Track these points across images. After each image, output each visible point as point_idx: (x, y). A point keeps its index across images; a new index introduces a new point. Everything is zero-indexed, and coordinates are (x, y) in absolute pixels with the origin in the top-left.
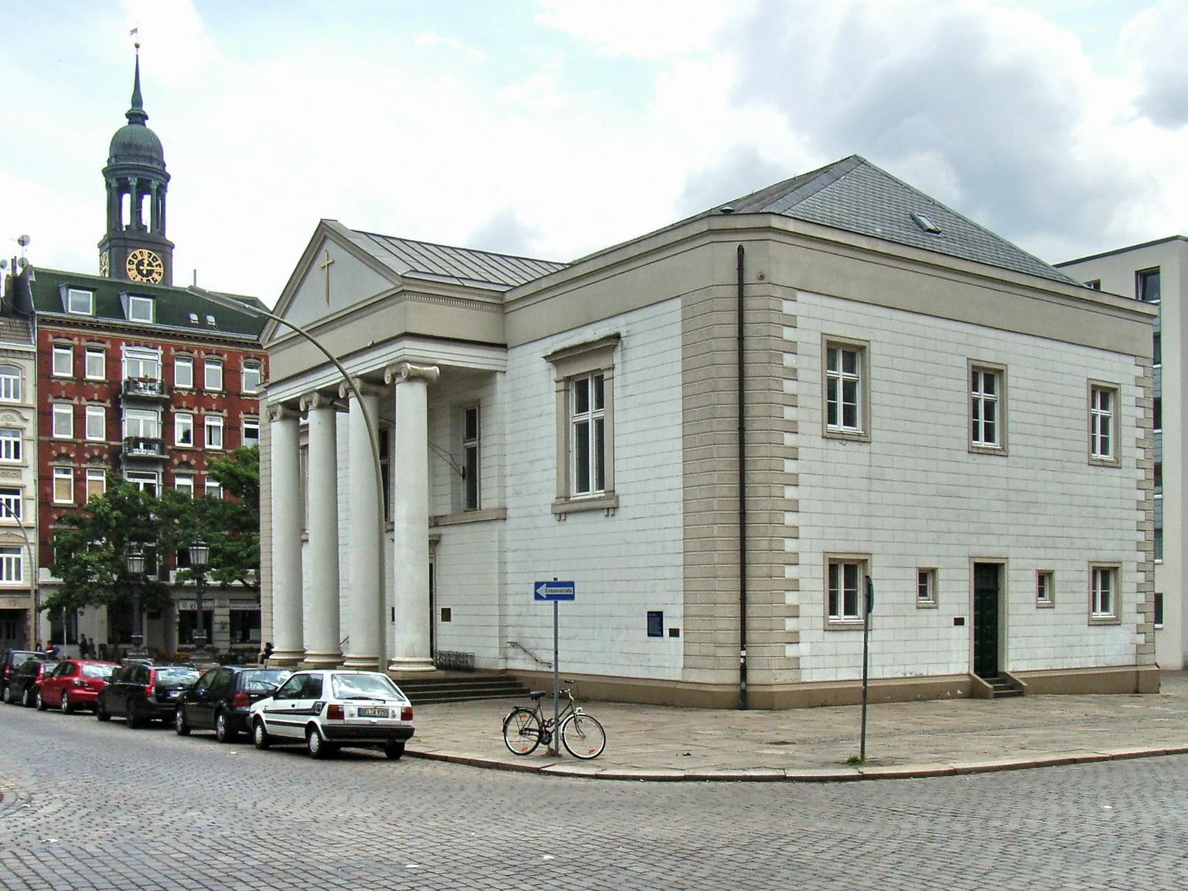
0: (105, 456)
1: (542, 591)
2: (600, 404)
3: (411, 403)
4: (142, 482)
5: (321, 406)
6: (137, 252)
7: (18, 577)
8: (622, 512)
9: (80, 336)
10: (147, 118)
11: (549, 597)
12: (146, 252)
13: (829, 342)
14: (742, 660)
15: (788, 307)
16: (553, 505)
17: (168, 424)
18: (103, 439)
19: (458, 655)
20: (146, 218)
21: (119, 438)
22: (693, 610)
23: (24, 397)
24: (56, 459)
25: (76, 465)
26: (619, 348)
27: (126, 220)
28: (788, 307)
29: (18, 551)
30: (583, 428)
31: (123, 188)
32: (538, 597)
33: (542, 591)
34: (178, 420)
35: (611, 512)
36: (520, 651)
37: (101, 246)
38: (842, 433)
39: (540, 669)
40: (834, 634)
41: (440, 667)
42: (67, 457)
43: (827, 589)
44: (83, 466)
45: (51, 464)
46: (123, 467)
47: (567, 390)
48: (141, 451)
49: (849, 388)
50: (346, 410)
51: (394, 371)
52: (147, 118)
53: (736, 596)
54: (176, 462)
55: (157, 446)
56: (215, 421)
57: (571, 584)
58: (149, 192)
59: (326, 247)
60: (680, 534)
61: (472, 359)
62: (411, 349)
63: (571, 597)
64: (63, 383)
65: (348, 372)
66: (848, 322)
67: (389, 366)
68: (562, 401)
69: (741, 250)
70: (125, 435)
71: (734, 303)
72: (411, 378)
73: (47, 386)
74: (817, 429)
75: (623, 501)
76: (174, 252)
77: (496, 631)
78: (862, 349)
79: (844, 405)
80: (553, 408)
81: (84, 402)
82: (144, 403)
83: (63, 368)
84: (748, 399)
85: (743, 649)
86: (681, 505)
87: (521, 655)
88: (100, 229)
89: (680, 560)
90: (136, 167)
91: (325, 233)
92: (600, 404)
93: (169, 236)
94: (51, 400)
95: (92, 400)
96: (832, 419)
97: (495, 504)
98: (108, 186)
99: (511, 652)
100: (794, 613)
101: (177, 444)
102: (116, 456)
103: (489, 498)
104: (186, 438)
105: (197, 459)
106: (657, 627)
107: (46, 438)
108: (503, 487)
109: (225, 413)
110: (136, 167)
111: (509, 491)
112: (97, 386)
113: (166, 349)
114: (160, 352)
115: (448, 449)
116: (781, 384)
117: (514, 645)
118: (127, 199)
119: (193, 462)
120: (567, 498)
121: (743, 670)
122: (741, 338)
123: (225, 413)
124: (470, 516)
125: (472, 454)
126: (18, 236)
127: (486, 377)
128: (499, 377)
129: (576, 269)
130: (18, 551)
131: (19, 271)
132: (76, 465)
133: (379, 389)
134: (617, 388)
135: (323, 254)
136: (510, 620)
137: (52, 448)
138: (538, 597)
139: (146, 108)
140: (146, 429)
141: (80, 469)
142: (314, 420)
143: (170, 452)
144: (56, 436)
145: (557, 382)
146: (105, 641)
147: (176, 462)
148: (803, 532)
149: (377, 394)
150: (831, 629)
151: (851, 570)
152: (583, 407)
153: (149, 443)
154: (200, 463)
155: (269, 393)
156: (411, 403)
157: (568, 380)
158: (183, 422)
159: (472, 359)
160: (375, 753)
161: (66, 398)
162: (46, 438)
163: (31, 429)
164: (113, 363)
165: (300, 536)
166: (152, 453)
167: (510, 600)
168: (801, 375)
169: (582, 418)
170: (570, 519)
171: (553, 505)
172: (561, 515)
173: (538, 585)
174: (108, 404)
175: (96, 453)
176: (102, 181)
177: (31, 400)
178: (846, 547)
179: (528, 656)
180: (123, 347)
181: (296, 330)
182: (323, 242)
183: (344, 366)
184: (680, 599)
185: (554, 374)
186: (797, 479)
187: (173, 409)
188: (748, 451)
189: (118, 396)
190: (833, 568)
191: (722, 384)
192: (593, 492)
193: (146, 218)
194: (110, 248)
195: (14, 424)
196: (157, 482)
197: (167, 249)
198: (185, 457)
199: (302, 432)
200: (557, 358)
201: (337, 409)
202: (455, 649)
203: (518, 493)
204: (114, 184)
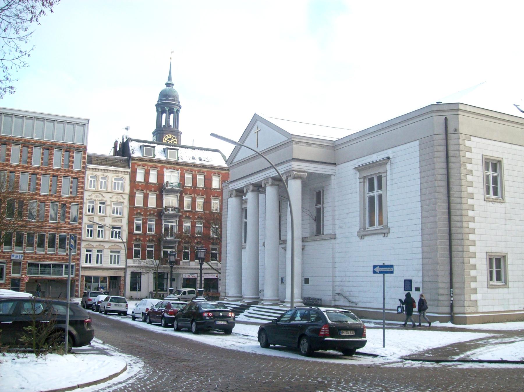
0: (156, 214)
1: (377, 269)
2: (380, 187)
3: (295, 188)
4: (170, 224)
5: (253, 191)
6: (167, 136)
7: (118, 263)
8: (390, 235)
9: (148, 165)
10: (173, 85)
11: (380, 273)
12: (171, 135)
13: (485, 159)
14: (451, 302)
15: (467, 143)
16: (358, 232)
17: (181, 201)
18: (155, 207)
19: (316, 299)
20: (171, 123)
21: (162, 206)
22: (427, 279)
23: (124, 190)
24: (135, 215)
25: (144, 217)
26: (389, 163)
27: (164, 123)
28: (467, 143)
29: (119, 252)
30: (372, 199)
31: (163, 111)
32: (375, 272)
33: (377, 269)
34: (185, 199)
35: (386, 235)
36: (341, 297)
37: (153, 133)
38: (493, 199)
39: (351, 305)
40: (492, 290)
41: (306, 304)
42: (140, 214)
43: (489, 270)
44: (147, 217)
45: (134, 217)
46: (163, 218)
47: (364, 182)
48: (171, 212)
49: (495, 179)
50: (264, 192)
51: (287, 175)
52: (173, 85)
53: (448, 273)
54: (184, 216)
55: (176, 210)
56: (200, 201)
57: (392, 266)
58: (173, 113)
59: (257, 124)
60: (420, 244)
61: (322, 170)
62: (296, 165)
63: (392, 272)
64: (140, 184)
65: (279, 171)
66: (495, 150)
67: (285, 173)
68: (362, 187)
69: (446, 119)
70: (164, 206)
71: (444, 142)
72: (295, 178)
73: (134, 186)
74: (482, 197)
75: (392, 230)
76: (182, 135)
77: (331, 288)
78: (500, 162)
79: (495, 188)
80: (358, 190)
81: (148, 192)
82: (171, 192)
83: (140, 177)
84: (451, 184)
85: (451, 297)
86: (421, 231)
87: (342, 299)
88: (154, 127)
89: (420, 256)
90: (167, 104)
91: (256, 119)
92: (380, 187)
93: (180, 129)
94: (135, 191)
95: (151, 191)
96: (488, 193)
97: (330, 232)
98: (157, 110)
99: (337, 297)
100: (474, 279)
101: (185, 209)
102: (160, 214)
103: (327, 229)
104: (188, 207)
105: (193, 215)
106: (409, 287)
107: (132, 206)
108: (334, 225)
109: (205, 196)
110: (167, 104)
111: (337, 227)
112: (153, 185)
113: (182, 170)
114: (179, 171)
115: (308, 209)
116: (466, 177)
117: (339, 294)
118: (164, 115)
119: (191, 216)
120: (365, 229)
121: (452, 306)
122: (447, 157)
123: (205, 196)
124: (318, 237)
125: (319, 212)
126: (126, 127)
127: (327, 177)
128: (333, 177)
129: (235, 183)
130: (119, 252)
131: (125, 140)
132: (144, 217)
133: (279, 182)
134: (388, 181)
135: (255, 127)
136: (337, 283)
137: (134, 210)
138: (375, 272)
139: (173, 81)
140: (172, 203)
141: (145, 219)
142: (250, 196)
143: (182, 212)
144: (136, 205)
145: (360, 179)
146: (152, 291)
147: (184, 216)
148: (477, 243)
149: (278, 185)
150: (490, 287)
151: (498, 260)
152: (371, 189)
153: (174, 209)
154: (194, 216)
155: (230, 186)
156: (295, 188)
157: (364, 178)
158: (187, 200)
159: (322, 170)
160: (332, 352)
161: (141, 190)
162: (132, 206)
163: (126, 202)
164: (160, 176)
165: (241, 247)
166: (175, 212)
167: (337, 274)
168: (474, 173)
169: (371, 194)
170: (366, 238)
171: (358, 232)
172: (362, 237)
173: (375, 267)
174: (158, 192)
175: (152, 212)
176: (155, 109)
177: (127, 191)
178: (497, 250)
179: (345, 300)
180: (165, 170)
181: (257, 152)
182: (256, 122)
183: (278, 168)
184: (420, 274)
185: (358, 175)
186: (474, 219)
187: (184, 195)
188: (452, 207)
189: (161, 189)
190: (491, 259)
191: (439, 177)
192: (377, 226)
193: (171, 123)
194: (157, 134)
195: (119, 200)
196: (175, 224)
197: (179, 134)
198: (188, 214)
199: (243, 202)
200: (359, 169)
201: (259, 192)
202: (311, 296)
203: (341, 227)
204: (160, 110)
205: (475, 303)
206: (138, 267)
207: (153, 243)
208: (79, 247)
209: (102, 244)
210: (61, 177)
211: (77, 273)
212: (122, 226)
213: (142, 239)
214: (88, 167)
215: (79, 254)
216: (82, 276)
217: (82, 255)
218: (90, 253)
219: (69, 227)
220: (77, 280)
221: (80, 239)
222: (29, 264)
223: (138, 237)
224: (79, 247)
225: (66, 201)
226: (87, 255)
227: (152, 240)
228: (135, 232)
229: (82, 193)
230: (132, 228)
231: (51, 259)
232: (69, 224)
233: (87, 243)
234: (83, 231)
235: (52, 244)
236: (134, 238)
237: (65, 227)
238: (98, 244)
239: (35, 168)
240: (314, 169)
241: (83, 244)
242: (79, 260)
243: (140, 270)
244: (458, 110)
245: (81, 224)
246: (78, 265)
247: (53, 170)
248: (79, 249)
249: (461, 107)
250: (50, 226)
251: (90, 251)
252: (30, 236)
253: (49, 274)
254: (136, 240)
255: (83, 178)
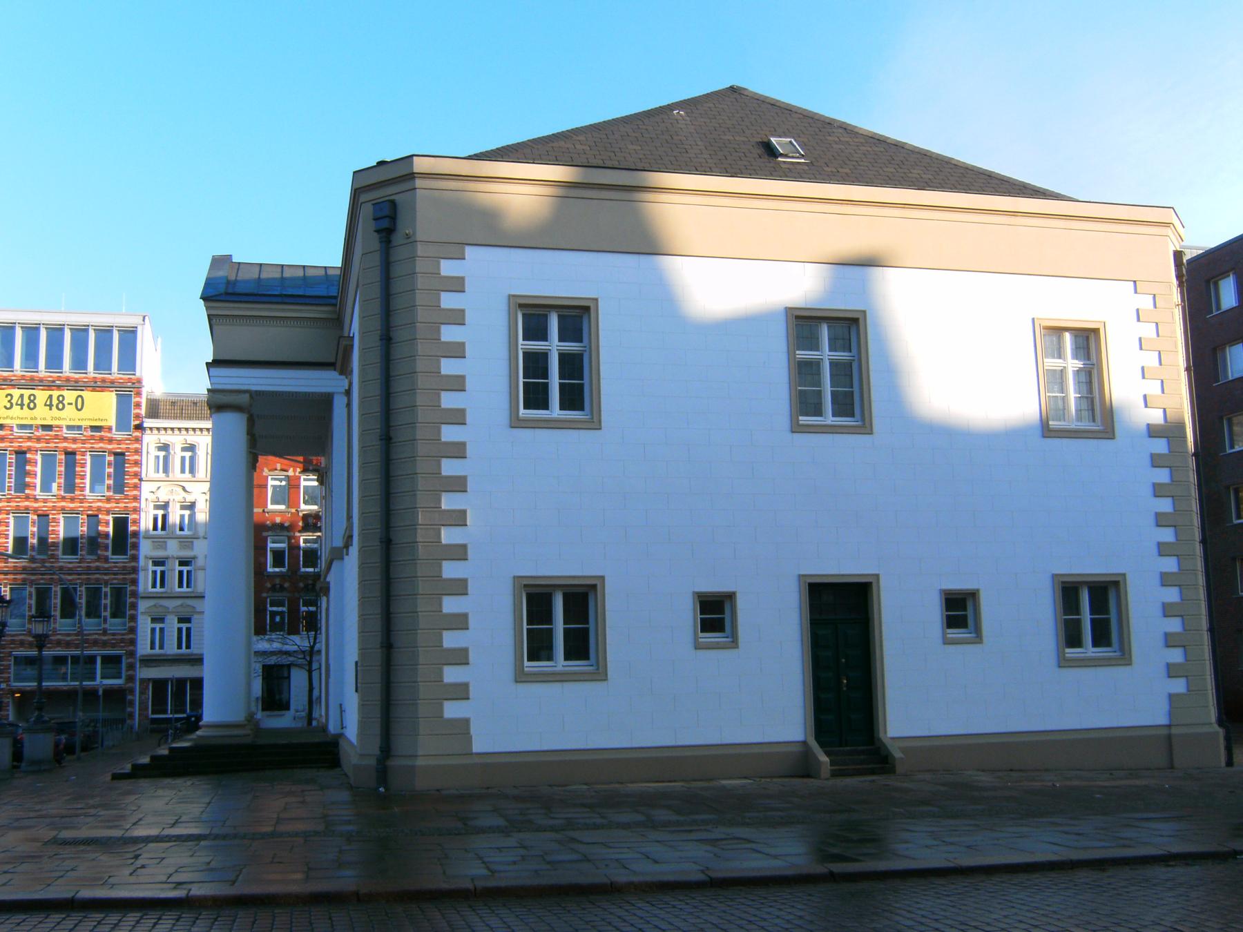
45: (265, 534)
61: (261, 381)
205: (462, 727)
206: (281, 652)
207: (285, 594)
208: (133, 612)
209: (189, 602)
210: (83, 454)
211: (130, 672)
212: (194, 558)
213: (286, 585)
214: (145, 425)
215: (133, 630)
216: (142, 681)
217: (140, 633)
218: (162, 625)
219: (106, 569)
220: (132, 691)
221: (135, 594)
222: (16, 658)
223: (277, 581)
224: (133, 612)
225: (99, 509)
226: (180, 630)
227: (282, 588)
228: (270, 570)
229: (137, 487)
230: (262, 560)
231: (68, 645)
232: (106, 560)
233: (152, 602)
234: (141, 575)
235: (93, 610)
236: (269, 585)
237: (98, 568)
238: (179, 602)
239: (20, 437)
240: (261, 381)
241: (143, 605)
242: (133, 642)
243: (285, 660)
244: (411, 176)
245: (135, 558)
246: (132, 654)
247: (65, 439)
248: (133, 618)
249: (420, 165)
250: (61, 568)
251: (161, 620)
252: (94, 594)
253: (64, 678)
254: (273, 589)
255: (138, 452)
